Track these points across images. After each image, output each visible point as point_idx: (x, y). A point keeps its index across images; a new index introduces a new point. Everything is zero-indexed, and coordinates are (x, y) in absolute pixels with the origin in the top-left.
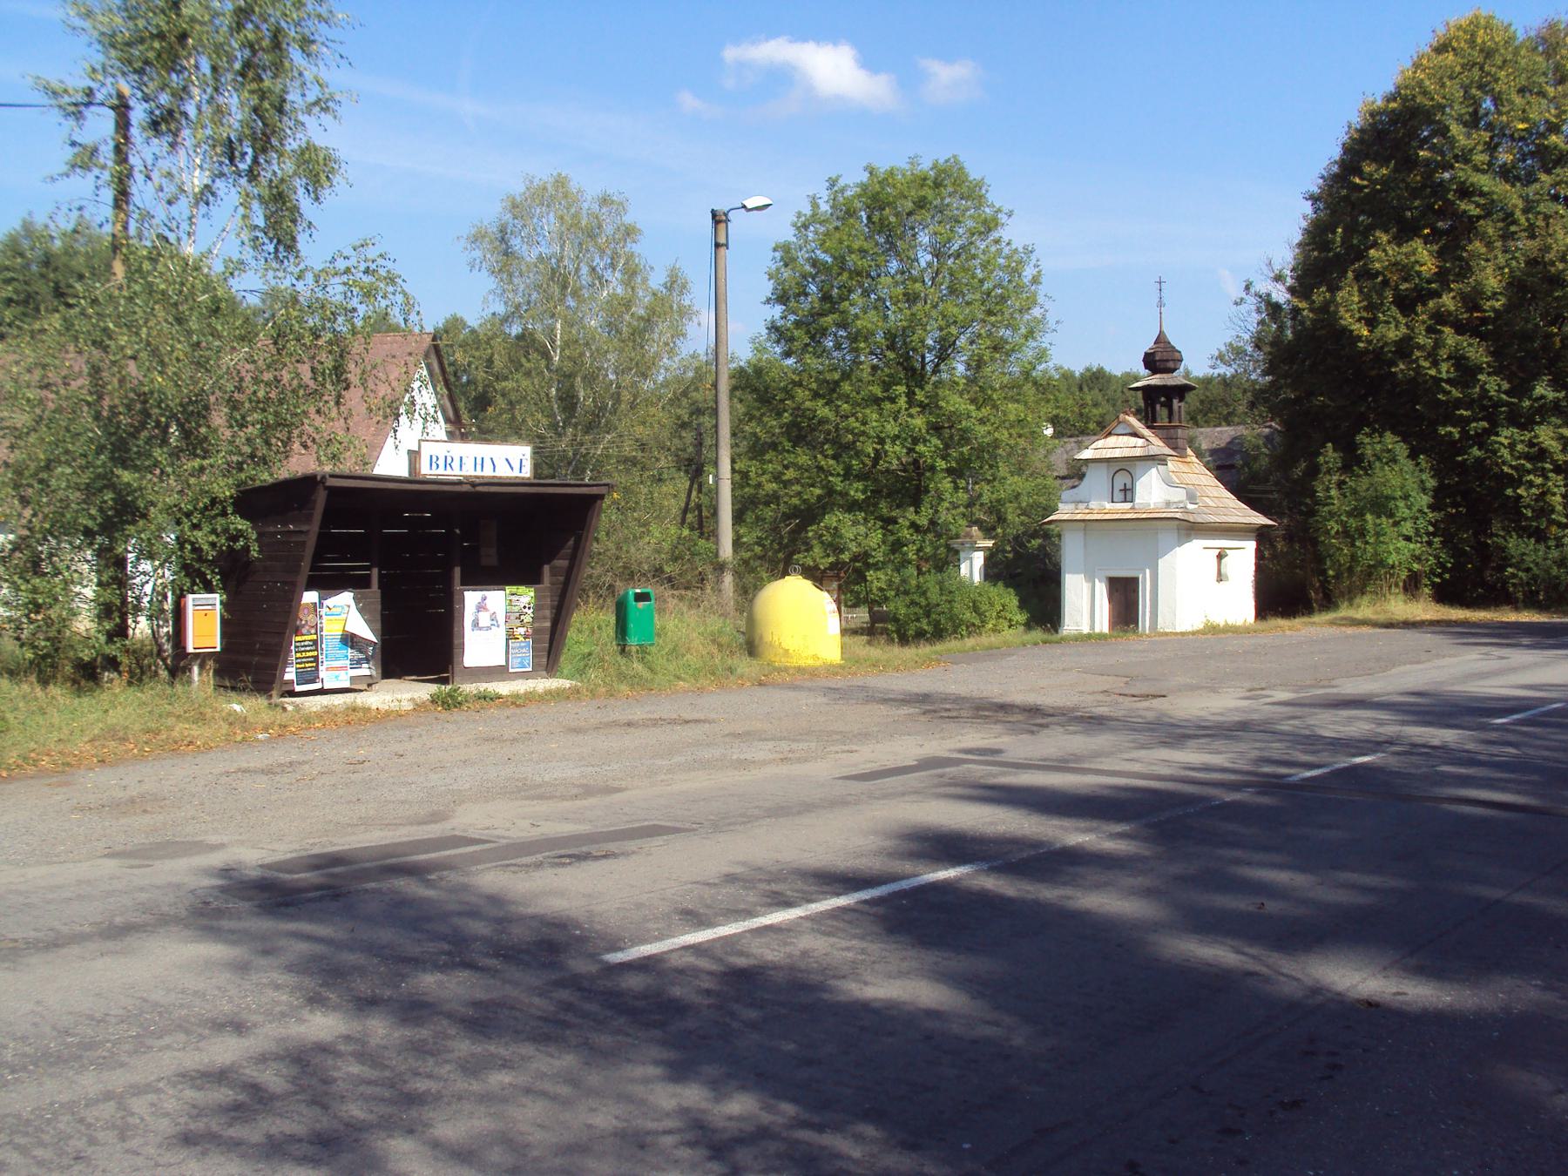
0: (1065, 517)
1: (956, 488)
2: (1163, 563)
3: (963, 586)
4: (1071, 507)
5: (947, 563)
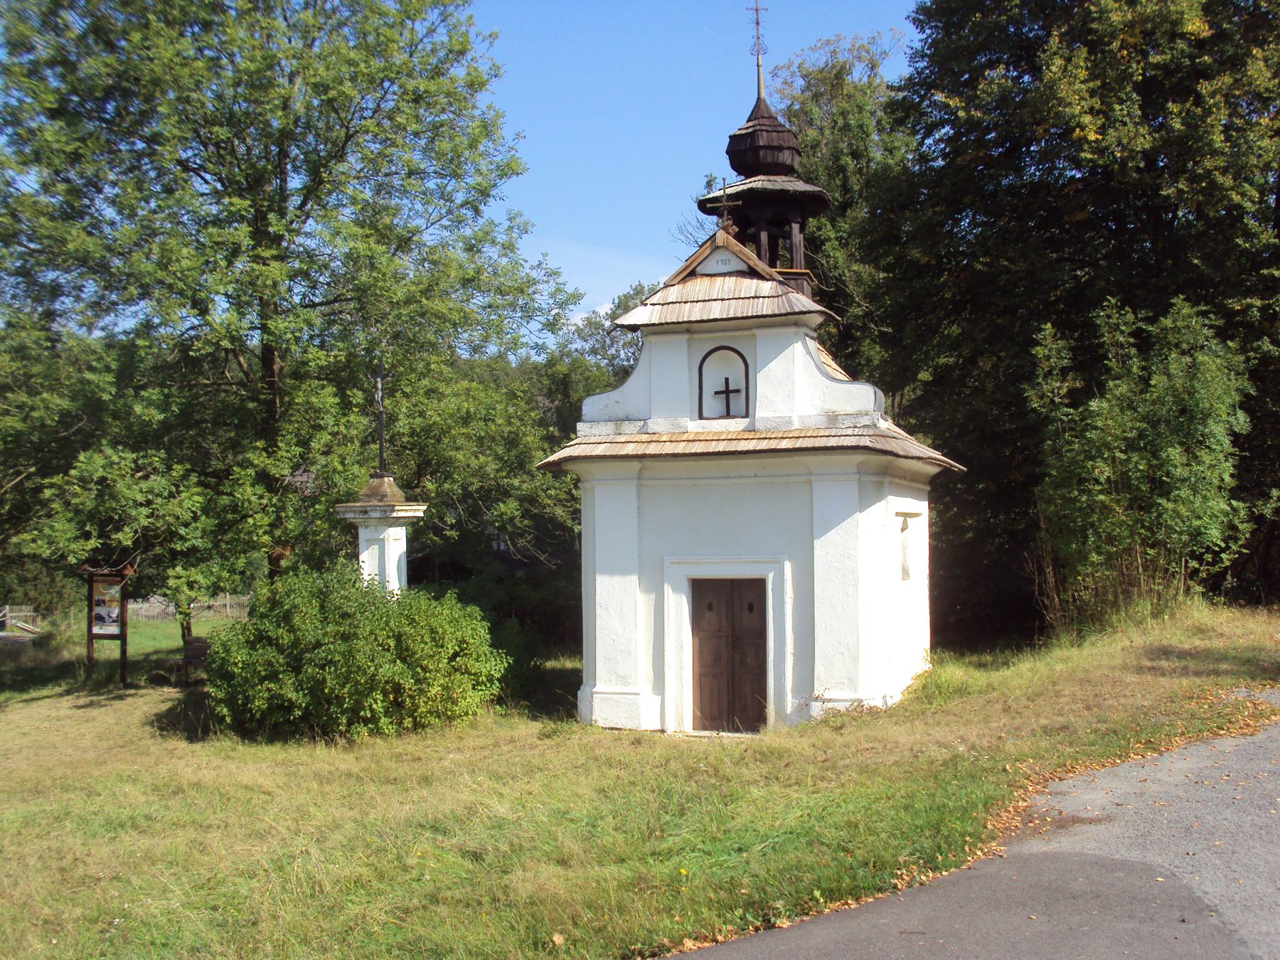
0: (600, 450)
1: (346, 406)
2: (826, 548)
3: (374, 598)
4: (606, 429)
5: (332, 554)
